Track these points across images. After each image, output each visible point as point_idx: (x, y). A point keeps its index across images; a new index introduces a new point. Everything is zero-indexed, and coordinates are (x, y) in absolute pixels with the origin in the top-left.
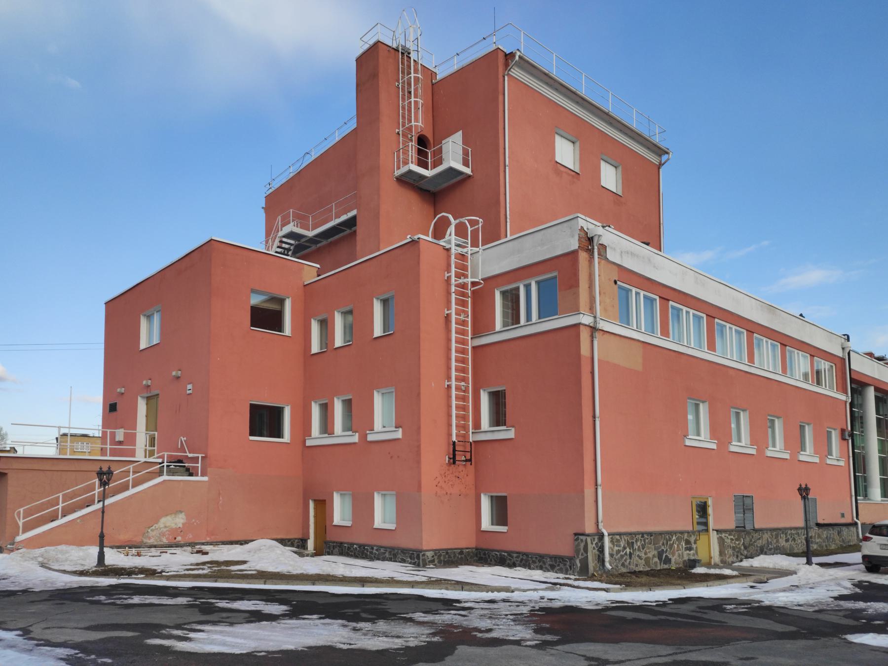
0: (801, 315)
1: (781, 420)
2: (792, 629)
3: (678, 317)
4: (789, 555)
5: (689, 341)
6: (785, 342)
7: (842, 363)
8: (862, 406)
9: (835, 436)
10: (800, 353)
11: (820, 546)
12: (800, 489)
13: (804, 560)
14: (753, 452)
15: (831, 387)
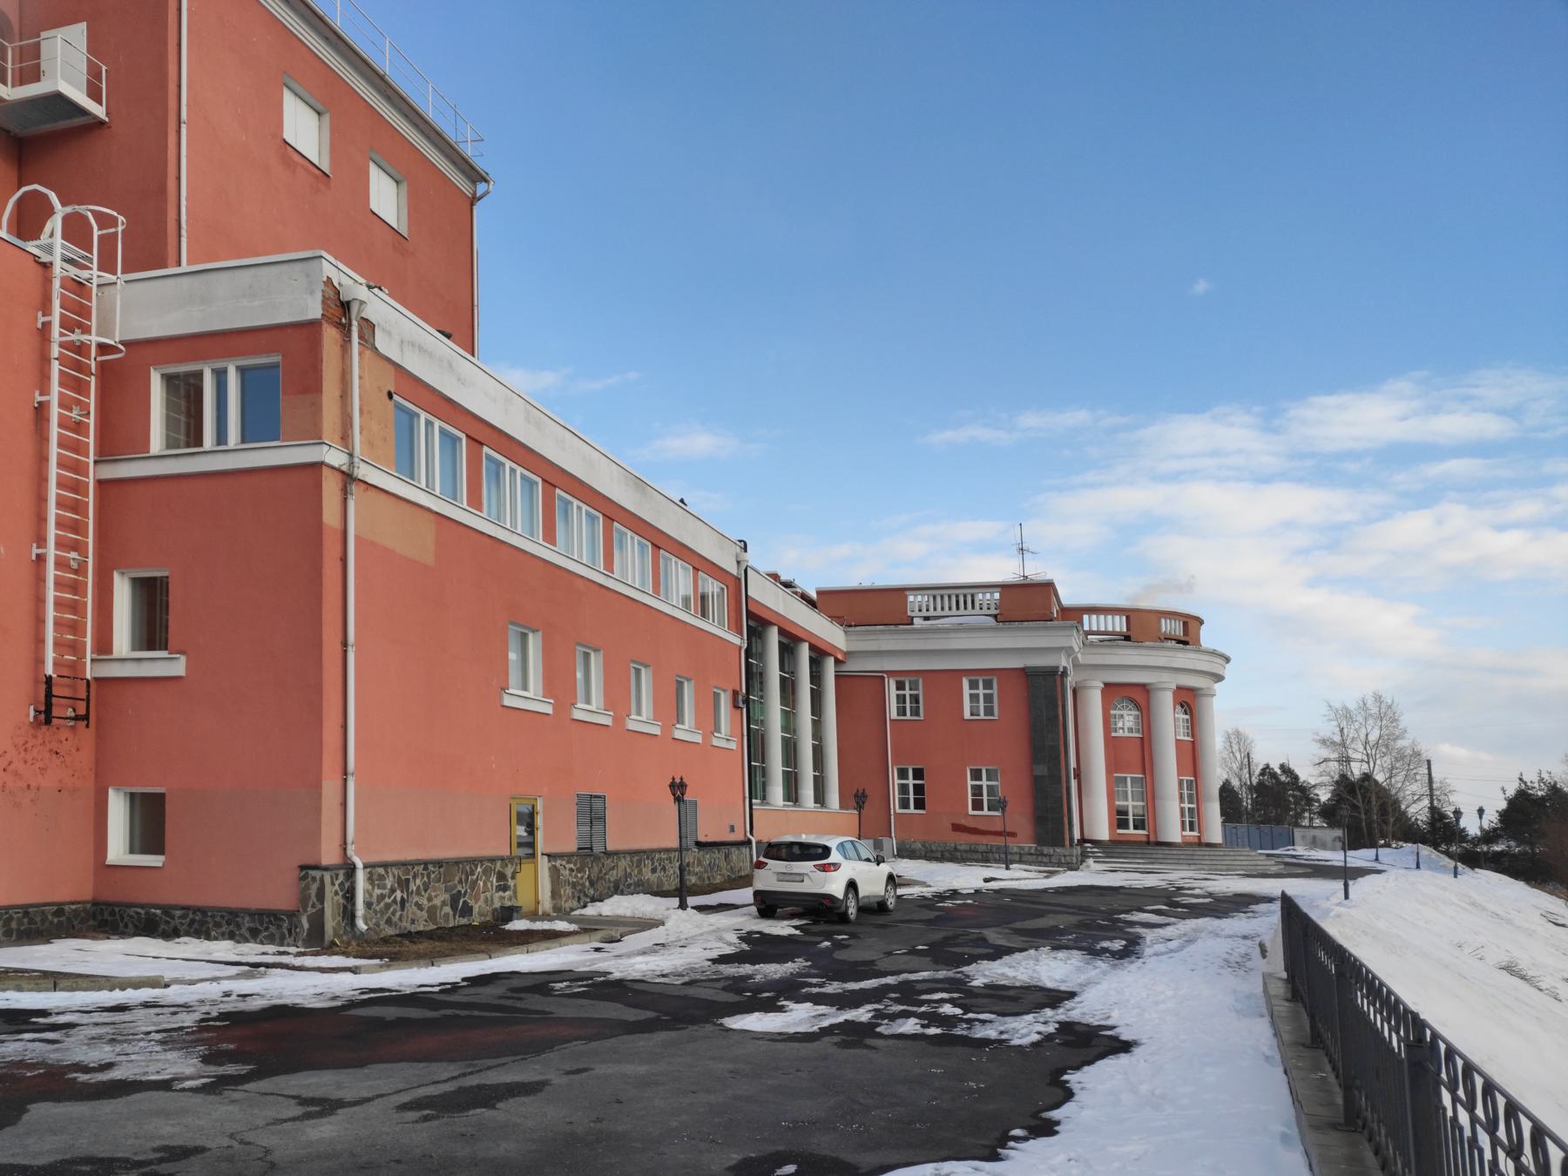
2: (651, 1014)
4: (655, 894)
7: (736, 584)
8: (762, 656)
9: (725, 701)
12: (672, 785)
13: (676, 901)
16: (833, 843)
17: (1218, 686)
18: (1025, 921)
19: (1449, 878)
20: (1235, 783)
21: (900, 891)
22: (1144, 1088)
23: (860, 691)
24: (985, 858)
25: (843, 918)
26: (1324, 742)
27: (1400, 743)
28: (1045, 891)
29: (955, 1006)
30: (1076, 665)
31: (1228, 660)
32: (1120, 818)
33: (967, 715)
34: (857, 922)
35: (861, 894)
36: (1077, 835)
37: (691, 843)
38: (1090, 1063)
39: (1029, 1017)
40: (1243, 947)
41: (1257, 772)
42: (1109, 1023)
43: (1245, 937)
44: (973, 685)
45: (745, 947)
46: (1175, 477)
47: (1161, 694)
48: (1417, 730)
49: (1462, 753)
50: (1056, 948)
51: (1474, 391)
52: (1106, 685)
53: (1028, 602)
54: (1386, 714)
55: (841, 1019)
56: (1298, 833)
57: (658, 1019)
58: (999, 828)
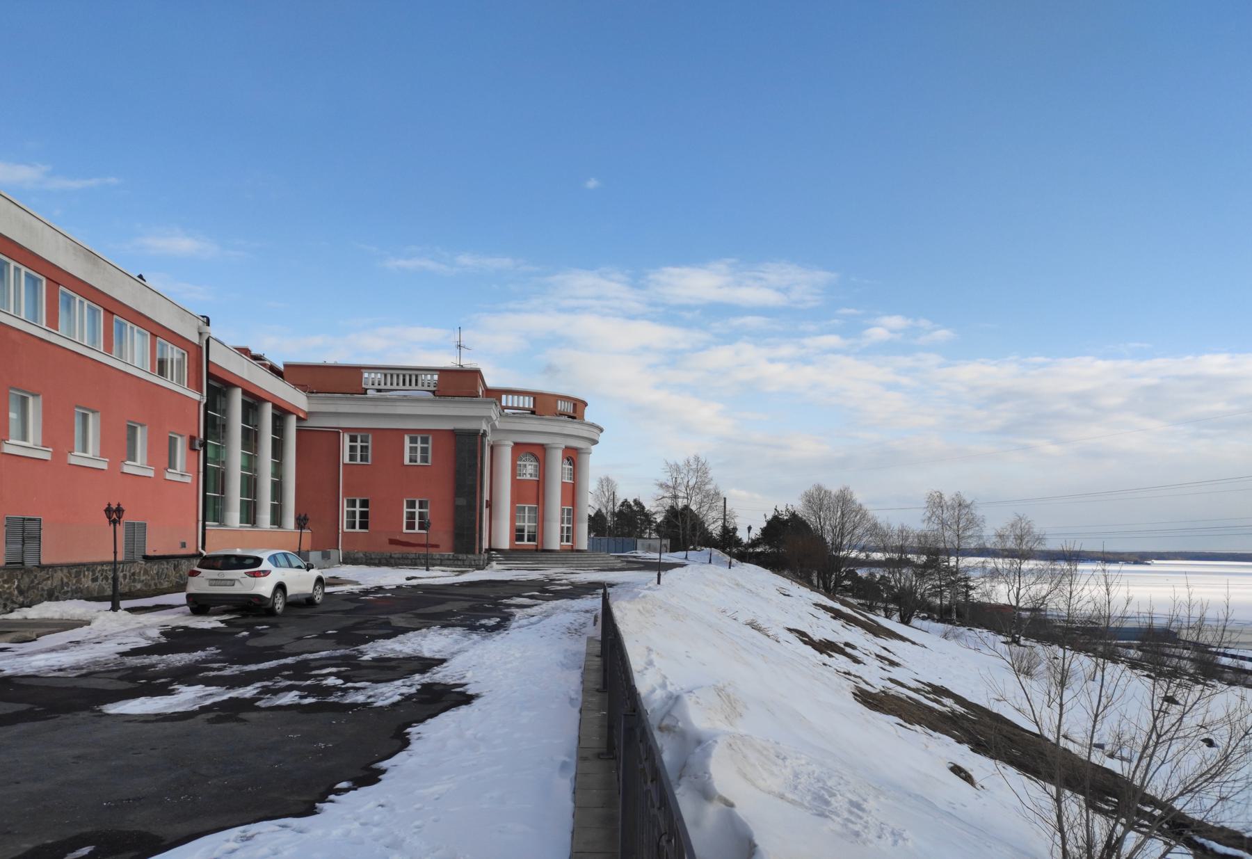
0: (140, 277)
1: (98, 416)
2: (24, 707)
3: (69, 306)
4: (88, 599)
5: (82, 337)
6: (112, 308)
7: (198, 353)
8: (225, 412)
9: (181, 446)
10: (136, 328)
11: (146, 585)
12: (108, 511)
13: (108, 605)
14: (47, 456)
15: (180, 381)
16: (265, 555)
17: (594, 448)
18: (424, 608)
19: (725, 569)
20: (604, 511)
21: (328, 590)
22: (469, 734)
23: (318, 444)
24: (413, 563)
25: (271, 612)
26: (661, 485)
27: (708, 487)
28: (452, 585)
29: (339, 678)
30: (494, 429)
31: (602, 430)
32: (518, 534)
33: (407, 461)
34: (284, 614)
35: (289, 593)
36: (485, 545)
37: (138, 556)
38: (435, 715)
39: (399, 683)
40: (582, 618)
41: (619, 503)
42: (463, 681)
43: (587, 612)
44: (413, 440)
45: (163, 640)
46: (572, 310)
47: (554, 451)
48: (719, 479)
49: (743, 493)
50: (444, 627)
51: (762, 275)
52: (516, 444)
53: (460, 383)
54: (700, 469)
55: (225, 697)
56: (640, 542)
57: (30, 710)
58: (424, 542)
